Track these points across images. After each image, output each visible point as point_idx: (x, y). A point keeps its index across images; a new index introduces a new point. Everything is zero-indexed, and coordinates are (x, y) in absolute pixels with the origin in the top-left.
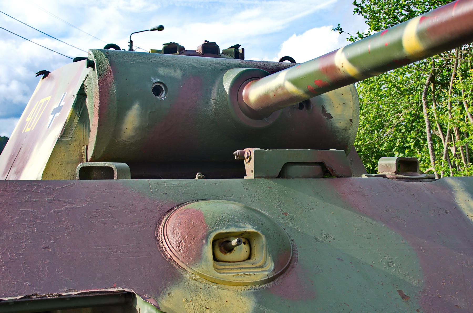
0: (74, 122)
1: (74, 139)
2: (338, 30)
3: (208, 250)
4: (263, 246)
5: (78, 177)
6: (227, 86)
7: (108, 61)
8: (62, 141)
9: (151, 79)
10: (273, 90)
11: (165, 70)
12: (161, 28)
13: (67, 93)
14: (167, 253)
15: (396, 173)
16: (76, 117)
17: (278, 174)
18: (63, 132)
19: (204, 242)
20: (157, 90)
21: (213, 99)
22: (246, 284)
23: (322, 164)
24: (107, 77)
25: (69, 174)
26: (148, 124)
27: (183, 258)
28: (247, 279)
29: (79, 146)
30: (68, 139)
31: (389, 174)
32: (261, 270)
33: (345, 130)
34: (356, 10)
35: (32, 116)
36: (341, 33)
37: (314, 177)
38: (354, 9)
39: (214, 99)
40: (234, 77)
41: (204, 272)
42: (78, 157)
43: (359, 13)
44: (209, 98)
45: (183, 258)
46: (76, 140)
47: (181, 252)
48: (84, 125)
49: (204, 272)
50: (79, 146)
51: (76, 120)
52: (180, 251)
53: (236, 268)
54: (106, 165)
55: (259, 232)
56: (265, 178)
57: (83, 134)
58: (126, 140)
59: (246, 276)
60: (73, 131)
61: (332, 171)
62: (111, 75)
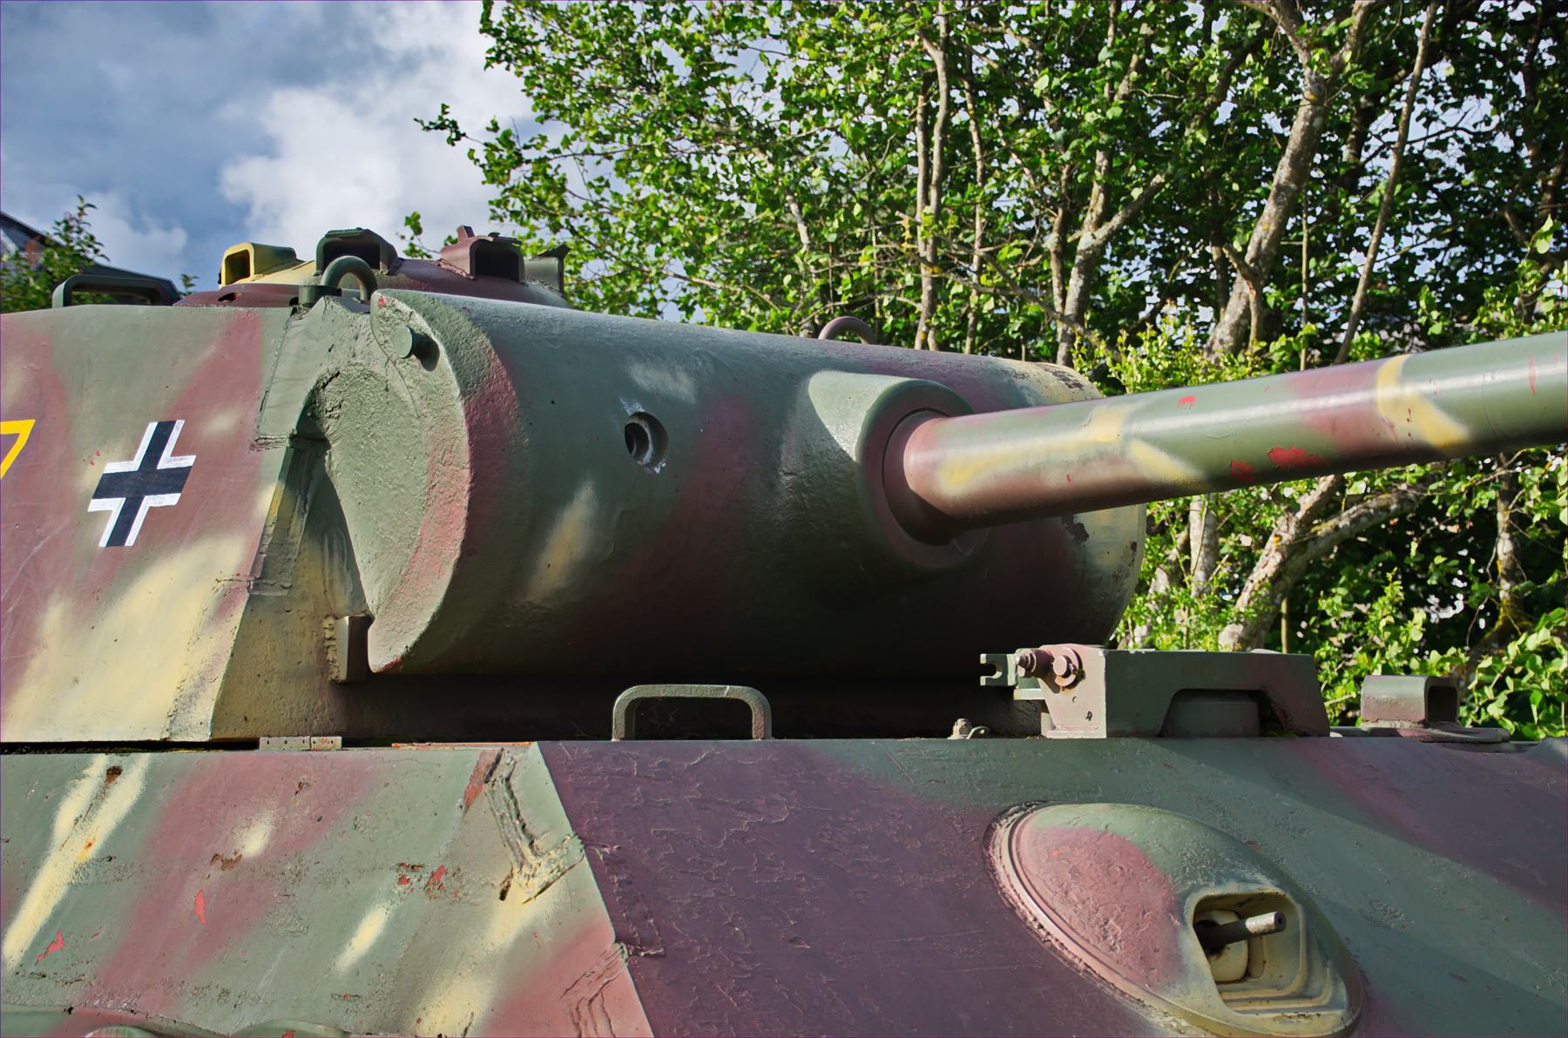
0: (291, 532)
1: (297, 594)
2: (441, 127)
3: (1191, 944)
4: (1297, 936)
5: (622, 729)
6: (848, 437)
7: (483, 340)
8: (261, 599)
9: (619, 402)
10: (1068, 464)
11: (648, 373)
13: (180, 424)
14: (1070, 957)
15: (1425, 724)
16: (296, 515)
17: (1161, 723)
18: (260, 567)
19: (1177, 922)
20: (634, 436)
21: (786, 474)
23: (1259, 697)
24: (492, 395)
25: (294, 715)
26: (611, 550)
27: (1130, 968)
29: (316, 618)
30: (279, 594)
31: (1405, 727)
32: (1310, 1005)
33: (1116, 577)
34: (493, 55)
36: (451, 142)
37: (1246, 735)
38: (489, 52)
39: (791, 474)
40: (869, 407)
41: (1199, 1009)
42: (315, 655)
43: (505, 64)
44: (775, 468)
45: (1130, 968)
46: (304, 597)
47: (1118, 950)
48: (322, 544)
49: (1199, 1009)
50: (316, 618)
51: (298, 526)
52: (1112, 949)
53: (1263, 999)
54: (724, 694)
55: (1288, 896)
56: (1128, 735)
57: (324, 575)
58: (537, 602)
59: (1302, 1020)
60: (293, 564)
61: (1286, 715)
62: (506, 386)
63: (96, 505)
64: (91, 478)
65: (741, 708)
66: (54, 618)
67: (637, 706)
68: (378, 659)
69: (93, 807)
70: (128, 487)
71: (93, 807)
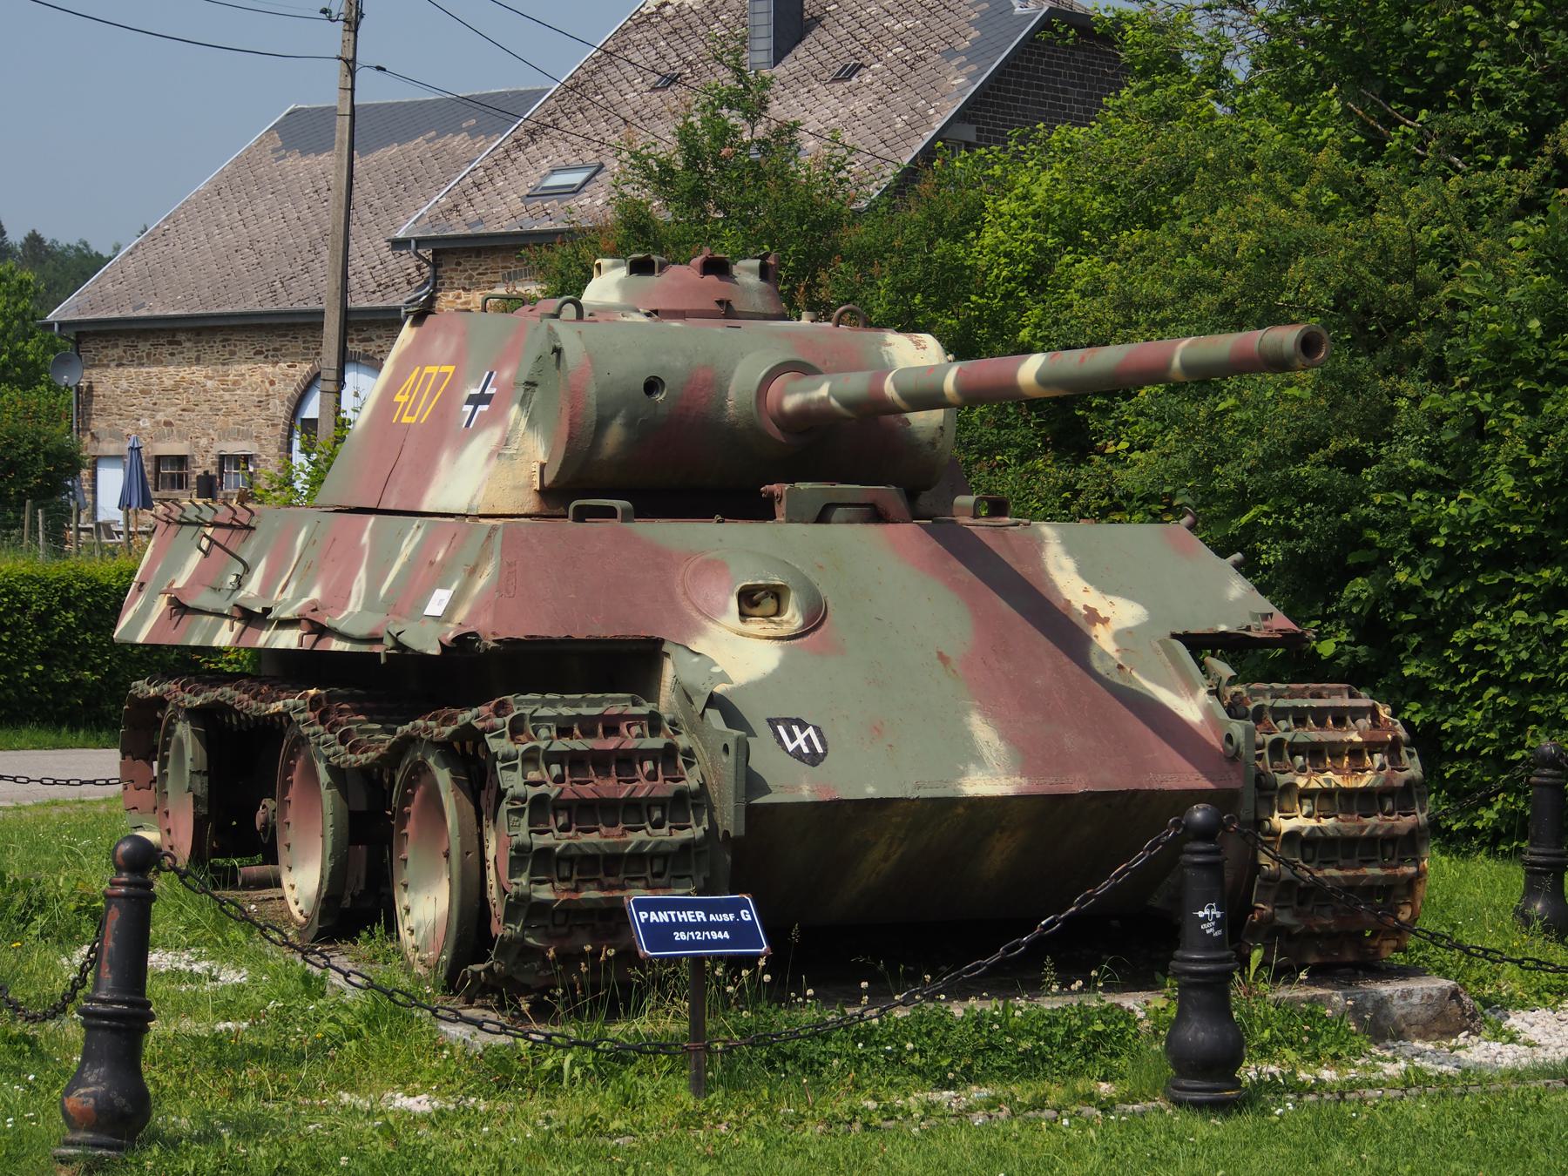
23: (872, 505)
35: (411, 394)
63: (493, 391)
64: (466, 396)
66: (444, 458)
67: (577, 508)
68: (547, 482)
69: (413, 537)
70: (475, 400)
71: (413, 537)
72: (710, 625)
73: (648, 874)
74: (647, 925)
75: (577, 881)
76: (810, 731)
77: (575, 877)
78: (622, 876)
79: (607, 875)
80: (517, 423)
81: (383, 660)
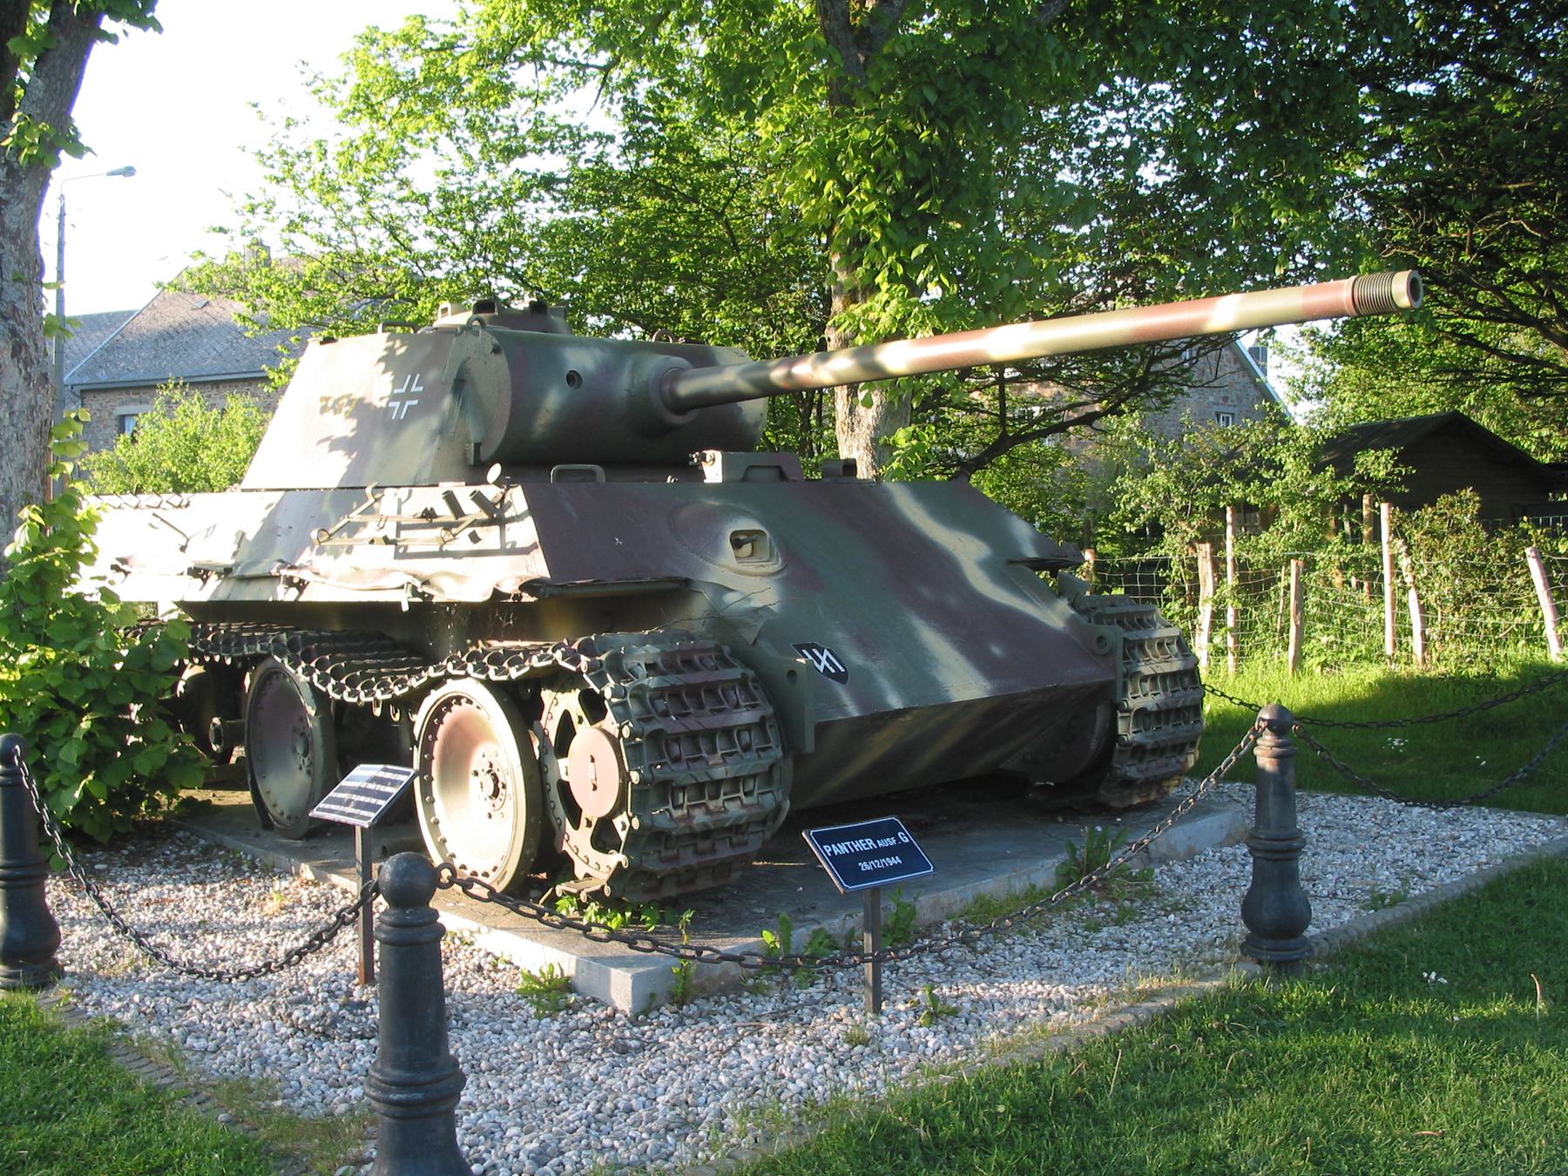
12: (129, 171)
22: (763, 575)
28: (762, 570)
51: (457, 412)
65: (592, 473)
72: (707, 564)
73: (741, 794)
74: (834, 858)
75: (689, 807)
76: (826, 653)
77: (686, 803)
78: (722, 797)
79: (711, 798)
80: (451, 411)
81: (405, 608)
